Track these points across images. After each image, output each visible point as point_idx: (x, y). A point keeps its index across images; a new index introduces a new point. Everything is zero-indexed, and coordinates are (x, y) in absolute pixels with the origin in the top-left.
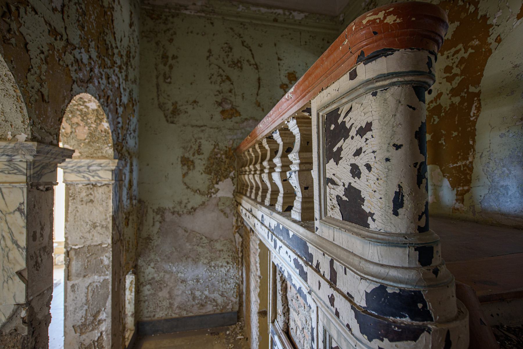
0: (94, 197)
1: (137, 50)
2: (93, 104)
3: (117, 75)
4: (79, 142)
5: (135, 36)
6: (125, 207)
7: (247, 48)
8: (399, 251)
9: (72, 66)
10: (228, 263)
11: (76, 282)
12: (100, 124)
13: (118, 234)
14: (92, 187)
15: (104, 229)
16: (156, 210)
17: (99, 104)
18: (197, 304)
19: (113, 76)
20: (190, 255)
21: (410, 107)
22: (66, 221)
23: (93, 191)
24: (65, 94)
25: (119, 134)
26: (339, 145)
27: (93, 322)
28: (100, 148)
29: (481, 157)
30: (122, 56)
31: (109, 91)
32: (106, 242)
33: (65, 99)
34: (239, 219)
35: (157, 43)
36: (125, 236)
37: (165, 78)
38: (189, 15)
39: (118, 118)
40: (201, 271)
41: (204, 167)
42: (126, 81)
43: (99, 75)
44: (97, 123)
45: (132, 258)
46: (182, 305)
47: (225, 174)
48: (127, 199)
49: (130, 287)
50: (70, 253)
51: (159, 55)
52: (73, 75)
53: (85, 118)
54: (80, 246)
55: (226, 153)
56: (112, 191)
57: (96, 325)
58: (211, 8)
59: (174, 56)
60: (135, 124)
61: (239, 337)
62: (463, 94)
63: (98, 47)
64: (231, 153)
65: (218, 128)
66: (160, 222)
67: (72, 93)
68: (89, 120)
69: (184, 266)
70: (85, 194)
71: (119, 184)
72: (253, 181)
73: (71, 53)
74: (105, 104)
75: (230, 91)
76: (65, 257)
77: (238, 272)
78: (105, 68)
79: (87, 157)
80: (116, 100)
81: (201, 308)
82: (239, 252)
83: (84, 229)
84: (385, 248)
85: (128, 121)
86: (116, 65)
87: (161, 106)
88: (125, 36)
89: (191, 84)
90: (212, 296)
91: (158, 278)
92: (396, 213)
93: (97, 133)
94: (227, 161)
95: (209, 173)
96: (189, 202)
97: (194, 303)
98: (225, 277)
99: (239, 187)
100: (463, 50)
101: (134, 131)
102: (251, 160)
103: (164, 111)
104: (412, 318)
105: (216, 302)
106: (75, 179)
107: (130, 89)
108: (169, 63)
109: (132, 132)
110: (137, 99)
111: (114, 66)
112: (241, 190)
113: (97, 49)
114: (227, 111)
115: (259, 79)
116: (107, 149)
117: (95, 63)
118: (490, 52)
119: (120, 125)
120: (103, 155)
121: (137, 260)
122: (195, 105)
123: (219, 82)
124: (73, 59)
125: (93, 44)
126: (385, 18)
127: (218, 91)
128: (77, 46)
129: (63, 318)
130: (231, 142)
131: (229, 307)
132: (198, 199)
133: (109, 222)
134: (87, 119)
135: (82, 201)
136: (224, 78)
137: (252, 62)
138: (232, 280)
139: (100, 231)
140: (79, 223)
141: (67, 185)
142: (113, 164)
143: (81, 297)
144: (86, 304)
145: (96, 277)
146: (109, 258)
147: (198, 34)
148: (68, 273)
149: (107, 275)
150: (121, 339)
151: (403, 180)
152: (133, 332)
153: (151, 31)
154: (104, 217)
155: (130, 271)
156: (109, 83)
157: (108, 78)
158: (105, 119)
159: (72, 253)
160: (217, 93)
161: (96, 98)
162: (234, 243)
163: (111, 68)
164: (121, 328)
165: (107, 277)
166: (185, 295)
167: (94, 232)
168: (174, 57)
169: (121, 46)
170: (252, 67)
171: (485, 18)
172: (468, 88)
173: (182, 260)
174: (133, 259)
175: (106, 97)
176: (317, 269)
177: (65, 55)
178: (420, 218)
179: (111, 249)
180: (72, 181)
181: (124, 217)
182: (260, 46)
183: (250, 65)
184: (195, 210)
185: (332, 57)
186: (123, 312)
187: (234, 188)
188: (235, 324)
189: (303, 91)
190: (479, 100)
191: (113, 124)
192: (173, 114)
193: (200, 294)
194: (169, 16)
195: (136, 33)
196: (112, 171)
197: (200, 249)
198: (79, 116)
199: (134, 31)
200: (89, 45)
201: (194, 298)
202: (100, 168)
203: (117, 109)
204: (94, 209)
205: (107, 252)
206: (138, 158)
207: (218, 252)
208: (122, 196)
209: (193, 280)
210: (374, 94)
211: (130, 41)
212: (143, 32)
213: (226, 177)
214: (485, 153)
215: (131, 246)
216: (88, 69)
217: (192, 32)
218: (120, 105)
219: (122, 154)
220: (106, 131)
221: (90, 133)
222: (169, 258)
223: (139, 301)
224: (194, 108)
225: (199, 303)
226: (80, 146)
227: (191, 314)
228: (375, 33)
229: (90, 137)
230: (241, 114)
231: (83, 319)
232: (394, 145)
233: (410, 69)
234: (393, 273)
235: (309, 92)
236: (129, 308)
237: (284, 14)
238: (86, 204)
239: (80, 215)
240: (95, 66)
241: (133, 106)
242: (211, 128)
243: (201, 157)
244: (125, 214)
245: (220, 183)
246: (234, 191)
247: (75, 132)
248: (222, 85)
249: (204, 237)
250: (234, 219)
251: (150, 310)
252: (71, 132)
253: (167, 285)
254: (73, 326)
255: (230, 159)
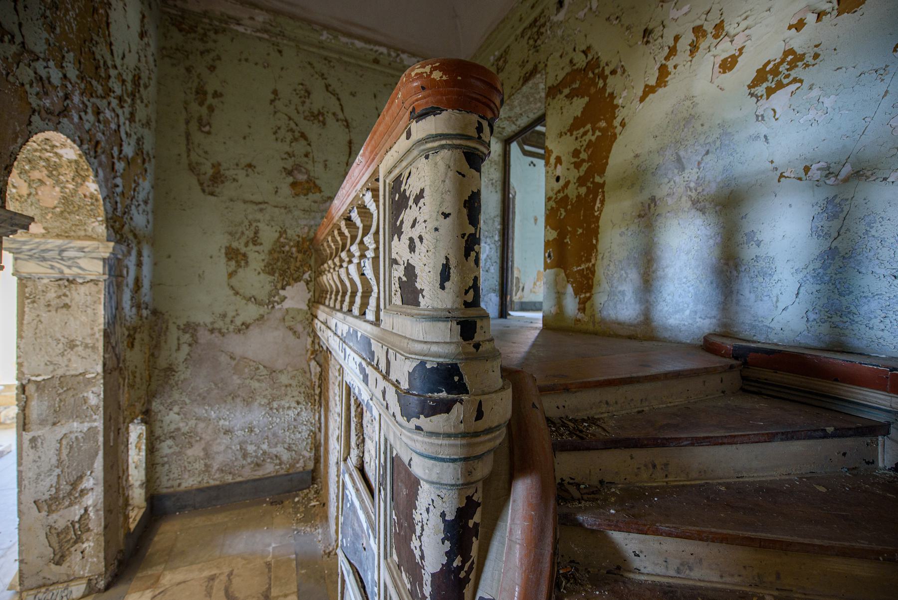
0: (71, 300)
1: (153, 76)
2: (70, 152)
3: (114, 110)
4: (45, 210)
5: (149, 54)
6: (128, 318)
7: (334, 95)
8: (441, 325)
9: (31, 85)
10: (298, 403)
11: (40, 433)
12: (82, 185)
13: (114, 358)
14: (66, 283)
15: (90, 350)
16: (182, 327)
17: (80, 152)
18: (249, 464)
19: (107, 111)
20: (240, 393)
21: (460, 173)
22: (20, 336)
23: (70, 290)
24: (18, 128)
25: (116, 203)
26: (400, 219)
27: (70, 494)
28: (81, 223)
29: (602, 258)
30: (124, 81)
31: (100, 134)
32: (92, 371)
33: (17, 137)
34: (317, 341)
35: (188, 70)
36: (127, 364)
37: (201, 123)
38: (243, 34)
39: (115, 177)
40: (257, 416)
41: (262, 264)
42: (130, 122)
43: (81, 106)
44: (77, 183)
45: (140, 398)
46: (225, 466)
47: (295, 276)
48: (132, 307)
49: (138, 442)
50: (27, 388)
51: (191, 89)
52: (33, 100)
53: (54, 173)
54: (46, 377)
55: (297, 244)
56: (103, 292)
57: (76, 498)
58: (279, 29)
59: (216, 92)
60: (146, 192)
61: (313, 503)
62: (589, 184)
63: (80, 63)
64: (305, 246)
65: (286, 208)
66: (190, 345)
67: (30, 128)
68: (61, 177)
69: (229, 410)
70: (54, 295)
71: (117, 281)
72: (331, 282)
73: (30, 66)
74: (92, 153)
75: (306, 155)
76: (17, 394)
77: (314, 415)
78: (92, 96)
79: (58, 236)
80: (112, 149)
81: (257, 468)
82: (316, 387)
83: (53, 350)
84: (429, 323)
85: (133, 186)
86: (112, 94)
87: (193, 168)
88: (130, 51)
89: (244, 138)
90: (274, 451)
91: (185, 429)
92: (442, 287)
93: (76, 199)
94: (300, 256)
95: (272, 273)
96: (238, 315)
97: (244, 462)
98: (295, 423)
99: (317, 295)
100: (590, 133)
101: (146, 202)
102: (331, 254)
103: (198, 175)
104: (448, 393)
105: (280, 459)
106: (37, 271)
107: (139, 135)
108: (208, 102)
109: (141, 203)
110: (150, 152)
111: (109, 95)
112: (318, 297)
113: (78, 66)
114: (301, 183)
115: (350, 142)
116: (94, 225)
117: (73, 86)
118: (614, 137)
119: (119, 190)
120: (88, 234)
121: (149, 402)
122: (250, 170)
123: (288, 140)
124: (33, 75)
125: (70, 56)
126: (431, 72)
127: (287, 153)
128: (42, 56)
129: (16, 490)
130: (306, 229)
131: (300, 465)
132: (251, 312)
133: (97, 340)
134: (59, 174)
135: (49, 305)
136: (297, 134)
137: (341, 116)
138: (304, 427)
139: (83, 353)
140: (43, 341)
141: (20, 279)
142: (106, 249)
143: (49, 455)
144: (58, 467)
145: (75, 424)
146: (99, 396)
147: (256, 64)
148: (25, 419)
149: (95, 420)
150: (122, 519)
151: (450, 251)
152: (143, 510)
153: (177, 49)
154: (90, 331)
155: (136, 418)
156: (99, 121)
157: (98, 112)
158: (92, 178)
159: (31, 389)
160: (286, 156)
161: (74, 141)
162: (308, 375)
163: (103, 98)
164: (121, 501)
165: (96, 424)
166: (230, 451)
167: (71, 355)
168: (216, 95)
169: (122, 65)
170: (340, 123)
171: (612, 96)
172: (594, 178)
173: (225, 401)
174: (143, 401)
175: (93, 143)
176: (377, 368)
177: (18, 67)
178: (467, 292)
179: (102, 381)
180: (30, 274)
181: (126, 333)
182: (353, 94)
183: (337, 120)
184: (248, 327)
185: (390, 111)
186: (124, 478)
187: (309, 296)
188: (309, 488)
189: (371, 152)
190: (603, 192)
191: (106, 186)
192: (215, 180)
193: (255, 448)
194: (209, 30)
195: (152, 49)
196: (104, 260)
197: (255, 384)
198: (44, 169)
199: (148, 45)
200: (63, 57)
201: (245, 456)
202: (82, 254)
203: (113, 164)
204: (72, 318)
205: (94, 386)
206: (152, 245)
207: (283, 388)
208: (121, 300)
209: (243, 429)
210: (427, 157)
211: (139, 60)
212: (164, 48)
213: (297, 280)
214: (607, 254)
215: (138, 380)
216: (61, 94)
217: (246, 60)
218: (119, 159)
219: (122, 236)
220: (92, 196)
221: (64, 198)
222: (204, 398)
223: (153, 465)
224: (247, 175)
225: (252, 462)
226: (45, 218)
227: (240, 479)
228: (423, 88)
229: (63, 204)
230: (323, 189)
231: (54, 490)
232: (443, 214)
233: (458, 132)
234: (434, 349)
235: (377, 154)
236: (136, 474)
237: (389, 55)
238: (56, 311)
239: (46, 329)
240: (73, 92)
241: (144, 162)
242: (275, 207)
243: (258, 248)
244: (128, 329)
245: (288, 288)
246: (309, 300)
247: (37, 194)
248: (293, 144)
249: (261, 367)
250: (310, 340)
251: (172, 476)
252: (29, 195)
253: (201, 438)
254: (35, 502)
255: (304, 254)
